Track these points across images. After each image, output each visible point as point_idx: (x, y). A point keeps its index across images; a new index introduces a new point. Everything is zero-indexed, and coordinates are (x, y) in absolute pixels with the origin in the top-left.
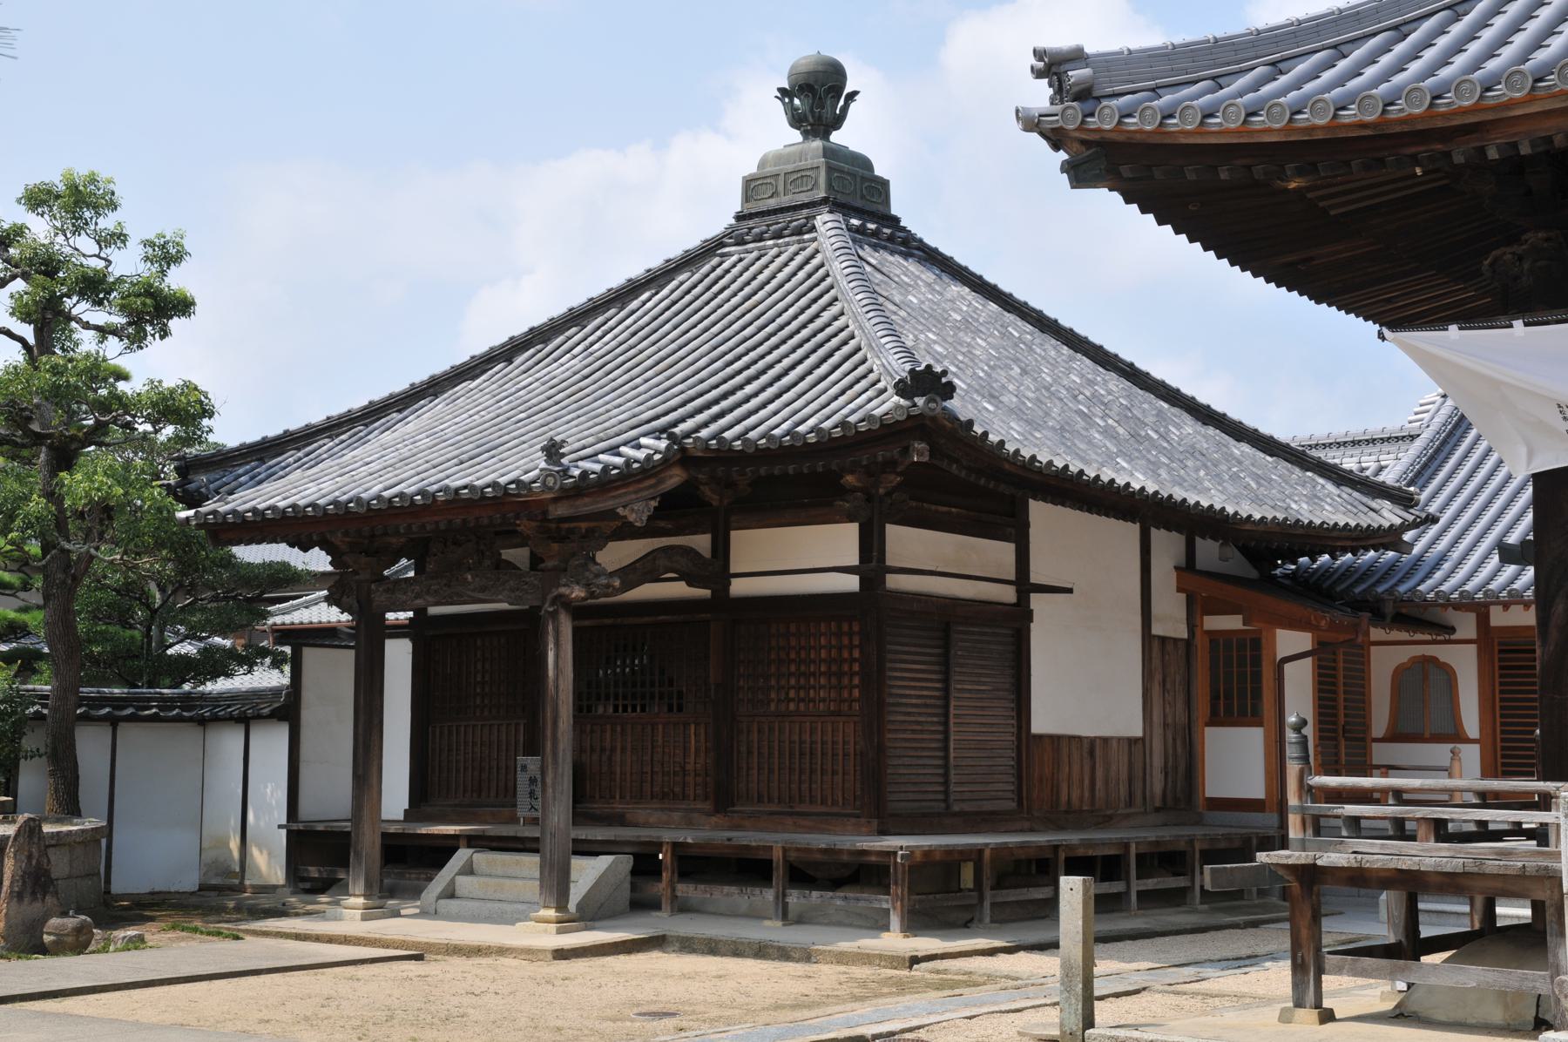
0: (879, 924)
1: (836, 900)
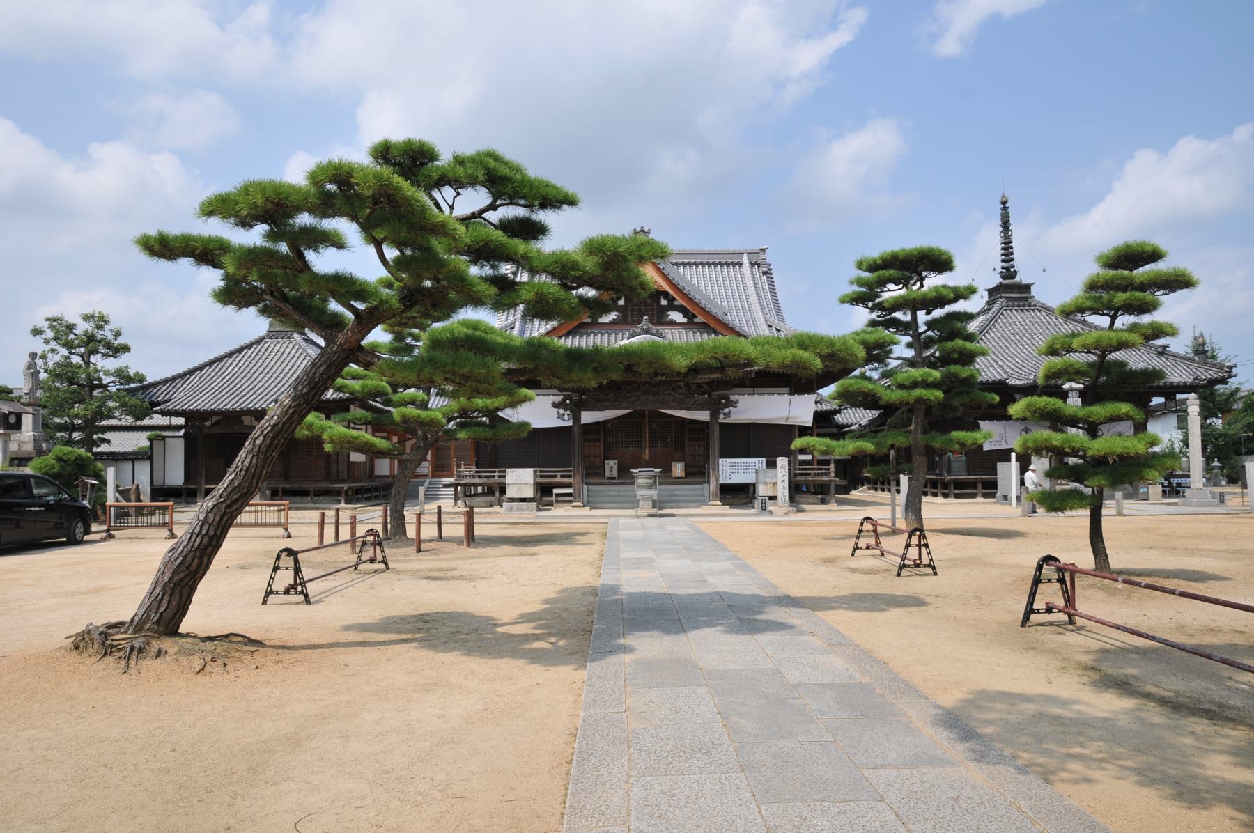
0: (339, 502)
1: (328, 498)
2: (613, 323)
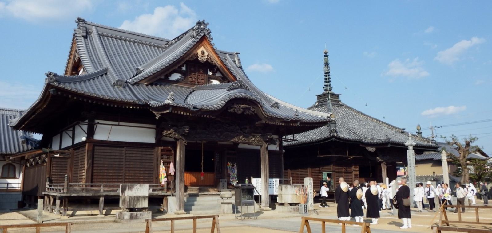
2: (177, 82)
